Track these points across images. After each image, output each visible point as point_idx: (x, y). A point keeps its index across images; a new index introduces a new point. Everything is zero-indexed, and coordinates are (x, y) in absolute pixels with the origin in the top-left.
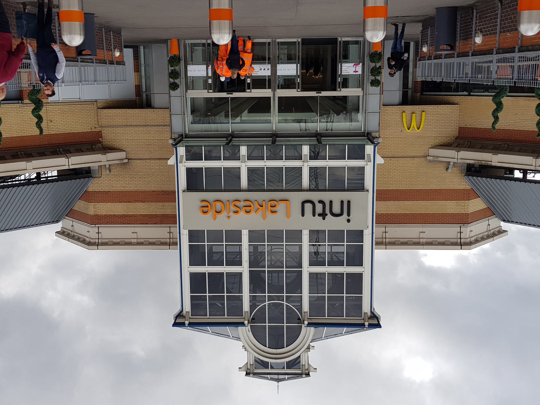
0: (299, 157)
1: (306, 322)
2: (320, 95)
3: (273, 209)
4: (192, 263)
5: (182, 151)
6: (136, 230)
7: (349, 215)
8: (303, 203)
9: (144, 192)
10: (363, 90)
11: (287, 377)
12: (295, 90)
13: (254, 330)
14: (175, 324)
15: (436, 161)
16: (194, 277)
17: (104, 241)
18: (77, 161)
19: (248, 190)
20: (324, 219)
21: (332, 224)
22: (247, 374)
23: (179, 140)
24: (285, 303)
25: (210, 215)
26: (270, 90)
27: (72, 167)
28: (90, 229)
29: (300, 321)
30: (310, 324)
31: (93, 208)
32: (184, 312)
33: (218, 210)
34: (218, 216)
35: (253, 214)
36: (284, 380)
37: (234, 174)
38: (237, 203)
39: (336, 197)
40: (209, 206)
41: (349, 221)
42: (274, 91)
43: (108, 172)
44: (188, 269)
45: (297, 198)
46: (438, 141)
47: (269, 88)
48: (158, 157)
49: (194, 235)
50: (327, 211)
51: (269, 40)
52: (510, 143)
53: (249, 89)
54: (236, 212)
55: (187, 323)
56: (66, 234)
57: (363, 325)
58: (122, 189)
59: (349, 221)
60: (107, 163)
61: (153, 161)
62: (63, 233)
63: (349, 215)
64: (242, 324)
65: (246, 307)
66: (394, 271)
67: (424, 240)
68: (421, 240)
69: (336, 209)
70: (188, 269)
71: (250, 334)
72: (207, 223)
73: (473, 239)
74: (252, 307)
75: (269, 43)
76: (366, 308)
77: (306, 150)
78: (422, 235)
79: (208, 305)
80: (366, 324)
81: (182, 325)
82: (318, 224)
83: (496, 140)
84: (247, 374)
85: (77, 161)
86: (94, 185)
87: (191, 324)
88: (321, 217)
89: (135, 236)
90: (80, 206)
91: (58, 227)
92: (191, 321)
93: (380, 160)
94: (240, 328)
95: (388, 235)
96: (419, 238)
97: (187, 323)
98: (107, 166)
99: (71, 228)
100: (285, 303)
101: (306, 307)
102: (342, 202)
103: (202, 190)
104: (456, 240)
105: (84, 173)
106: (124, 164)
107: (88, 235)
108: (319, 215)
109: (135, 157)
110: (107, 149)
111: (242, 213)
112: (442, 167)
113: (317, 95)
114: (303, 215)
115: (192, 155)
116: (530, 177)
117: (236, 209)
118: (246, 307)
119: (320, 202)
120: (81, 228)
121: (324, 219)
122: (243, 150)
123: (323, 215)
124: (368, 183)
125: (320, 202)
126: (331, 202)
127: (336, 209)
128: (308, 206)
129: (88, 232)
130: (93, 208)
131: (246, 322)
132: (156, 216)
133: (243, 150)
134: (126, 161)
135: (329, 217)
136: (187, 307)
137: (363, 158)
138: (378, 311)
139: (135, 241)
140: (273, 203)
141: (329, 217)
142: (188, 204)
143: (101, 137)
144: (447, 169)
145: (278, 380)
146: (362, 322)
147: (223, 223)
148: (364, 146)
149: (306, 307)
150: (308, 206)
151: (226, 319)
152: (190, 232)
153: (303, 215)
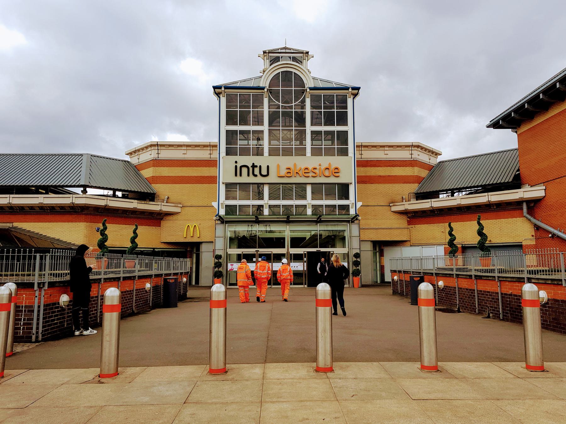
1: (266, 90)
3: (289, 171)
5: (352, 212)
6: (385, 156)
7: (236, 166)
8: (268, 175)
10: (227, 253)
11: (280, 51)
13: (303, 85)
14: (358, 89)
15: (176, 204)
16: (345, 123)
17: (408, 149)
18: (426, 204)
20: (253, 164)
21: (248, 160)
22: (307, 53)
23: (354, 219)
24: (281, 104)
26: (291, 253)
27: (429, 200)
28: (417, 157)
29: (270, 91)
32: (352, 97)
33: (327, 170)
34: (327, 166)
36: (281, 49)
38: (314, 175)
39: (245, 179)
41: (236, 162)
42: (288, 252)
43: (404, 197)
46: (170, 218)
47: (291, 254)
50: (251, 169)
55: (350, 90)
57: (226, 88)
58: (394, 185)
59: (236, 162)
62: (437, 154)
63: (236, 166)
64: (311, 89)
67: (183, 148)
68: (185, 148)
69: (245, 170)
71: (305, 82)
72: (336, 161)
73: (150, 149)
74: (303, 101)
76: (223, 100)
77: (266, 212)
79: (335, 104)
80: (223, 89)
81: (354, 89)
84: (307, 53)
85: (426, 204)
86: (414, 188)
87: (347, 89)
89: (386, 152)
90: (424, 173)
93: (215, 204)
94: (313, 86)
95: (209, 152)
97: (350, 90)
100: (281, 104)
101: (266, 101)
102: (241, 175)
103: (338, 184)
105: (420, 196)
106: (393, 202)
107: (419, 153)
108: (256, 166)
110: (405, 213)
111: (310, 168)
112: (171, 199)
114: (268, 166)
116: (111, 193)
117: (315, 171)
119: (256, 176)
120: (424, 158)
121: (253, 164)
123: (254, 166)
124: (223, 188)
125: (256, 176)
126: (248, 175)
127: (245, 170)
128: (264, 172)
131: (308, 90)
132: (371, 166)
133: (309, 212)
134: (391, 205)
135: (250, 165)
136: (350, 101)
138: (215, 98)
139: (386, 149)
140: (289, 175)
141: (250, 165)
142: (347, 171)
144: (168, 198)
145: (285, 48)
146: (226, 90)
147: (324, 161)
149: (266, 101)
150: (264, 172)
151: (322, 93)
153: (268, 166)
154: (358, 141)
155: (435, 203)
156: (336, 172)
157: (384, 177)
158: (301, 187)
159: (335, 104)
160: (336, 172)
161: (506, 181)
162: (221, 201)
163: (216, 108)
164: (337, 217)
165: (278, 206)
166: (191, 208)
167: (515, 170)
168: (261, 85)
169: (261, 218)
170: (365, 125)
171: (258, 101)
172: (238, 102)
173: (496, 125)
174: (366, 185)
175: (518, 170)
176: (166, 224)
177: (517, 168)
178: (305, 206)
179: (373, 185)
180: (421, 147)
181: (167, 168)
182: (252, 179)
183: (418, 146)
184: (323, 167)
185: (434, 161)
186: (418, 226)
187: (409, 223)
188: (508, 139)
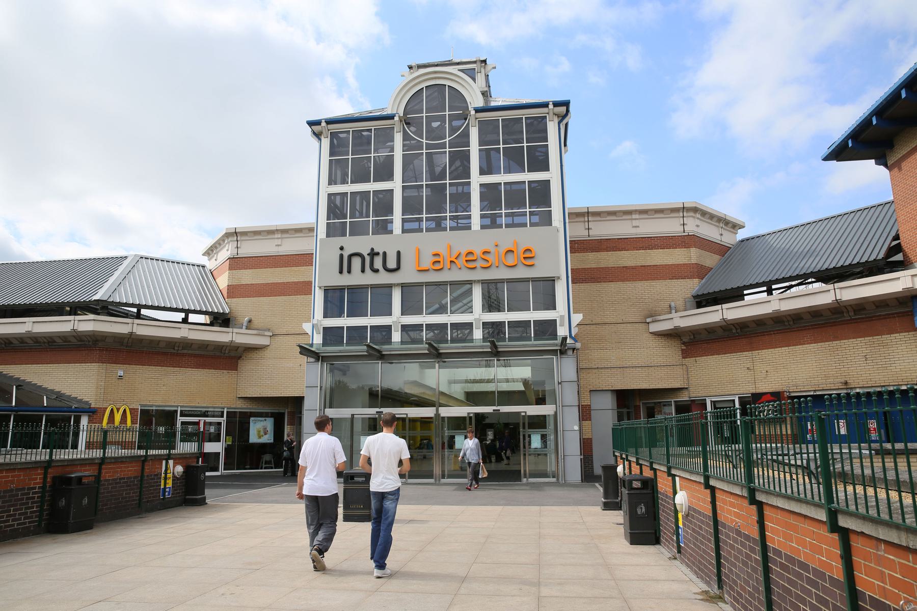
0: (405, 328)
1: (396, 118)
2: (495, 408)
3: (437, 259)
4: (546, 184)
5: (562, 331)
7: (341, 256)
8: (398, 268)
9: (624, 280)
12: (528, 414)
14: (566, 104)
15: (261, 331)
16: (544, 165)
18: (713, 315)
19: (470, 282)
20: (372, 249)
21: (362, 244)
22: (485, 61)
24: (424, 141)
25: (522, 248)
26: (442, 415)
27: (718, 307)
28: (695, 229)
30: (391, 117)
31: (693, 256)
32: (556, 120)
33: (510, 255)
34: (510, 247)
35: (464, 251)
37: (491, 305)
38: (485, 265)
39: (357, 278)
40: (523, 261)
41: (342, 248)
42: (437, 415)
43: (673, 304)
44: (552, 175)
45: (408, 275)
46: (255, 355)
47: (443, 418)
48: (607, 326)
49: (546, 219)
50: (368, 259)
51: (443, 481)
52: (172, 351)
53: (470, 418)
54: (485, 252)
56: (730, 225)
57: (329, 122)
58: (654, 283)
59: (342, 248)
60: (674, 315)
61: (614, 321)
62: (735, 226)
63: (341, 256)
64: (477, 110)
65: (474, 134)
66: (295, 191)
67: (276, 236)
68: (279, 236)
69: (356, 262)
70: (552, 175)
71: (468, 100)
72: (526, 237)
75: (443, 477)
76: (326, 142)
77: (396, 337)
78: (279, 242)
79: (525, 135)
81: (557, 104)
82: (379, 243)
83: (190, 355)
84: (485, 61)
85: (713, 315)
86: (693, 286)
87: (545, 105)
88: (376, 251)
89: (635, 223)
90: (711, 260)
91: (741, 235)
92: (545, 110)
96: (282, 238)
98: (673, 311)
99: (724, 232)
100: (424, 141)
101: (398, 138)
102: (349, 272)
103: (535, 280)
104: (243, 238)
105: (703, 301)
107: (698, 222)
108: (378, 254)
109: (637, 325)
111: (478, 251)
112: (256, 322)
113: (498, 408)
114: (399, 253)
115: (547, 329)
116: (180, 316)
117: (486, 257)
118: (474, 134)
119: (377, 271)
120: (710, 232)
121: (372, 249)
122: (478, 334)
123: (373, 254)
124: (319, 297)
125: (377, 271)
126: (363, 271)
127: (356, 262)
128: (392, 264)
129: (698, 226)
130: (693, 256)
132: (607, 249)
133: (478, 334)
134: (648, 320)
135: (365, 252)
137: (326, 329)
138: (314, 141)
139: (634, 216)
140: (438, 267)
141: (365, 252)
142: (554, 261)
143: (682, 350)
144: (250, 321)
146: (330, 126)
147: (505, 237)
148: (325, 343)
149: (398, 138)
150: (392, 264)
152: (551, 225)
153: (399, 253)
154: (576, 202)
155: (731, 312)
156: (528, 256)
157: (633, 268)
158: (462, 289)
159: (525, 135)
160: (528, 256)
161: (872, 259)
162: (314, 321)
163: (313, 157)
164: (533, 344)
165: (418, 327)
166: (287, 337)
167: (890, 238)
168: (388, 112)
169: (385, 349)
170: (591, 175)
171: (386, 137)
172: (349, 142)
173: (840, 153)
174: (598, 285)
175: (897, 237)
176: (247, 366)
177: (893, 234)
178: (469, 325)
179: (612, 285)
180: (701, 210)
181: (250, 271)
182: (369, 279)
183: (695, 210)
184: (503, 250)
185: (729, 239)
186: (702, 360)
187: (686, 354)
188: (867, 179)
